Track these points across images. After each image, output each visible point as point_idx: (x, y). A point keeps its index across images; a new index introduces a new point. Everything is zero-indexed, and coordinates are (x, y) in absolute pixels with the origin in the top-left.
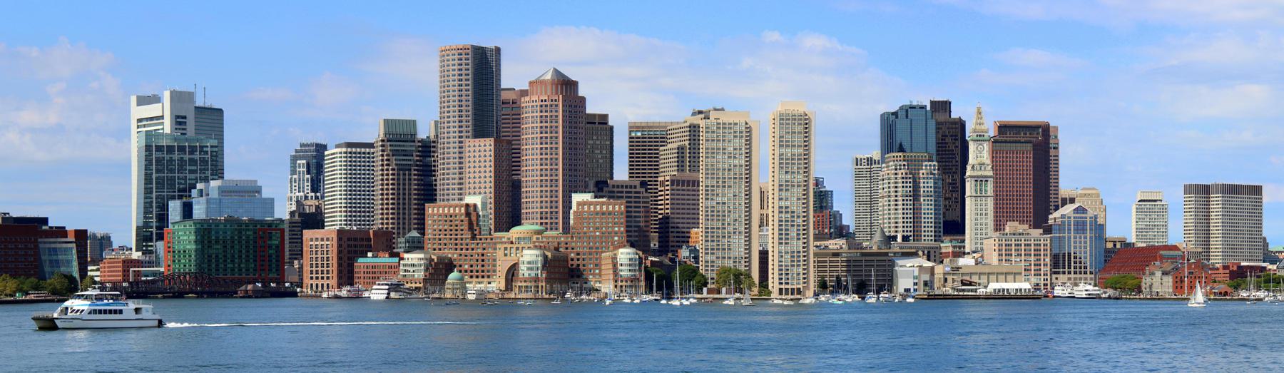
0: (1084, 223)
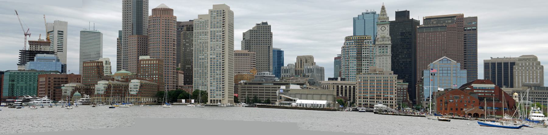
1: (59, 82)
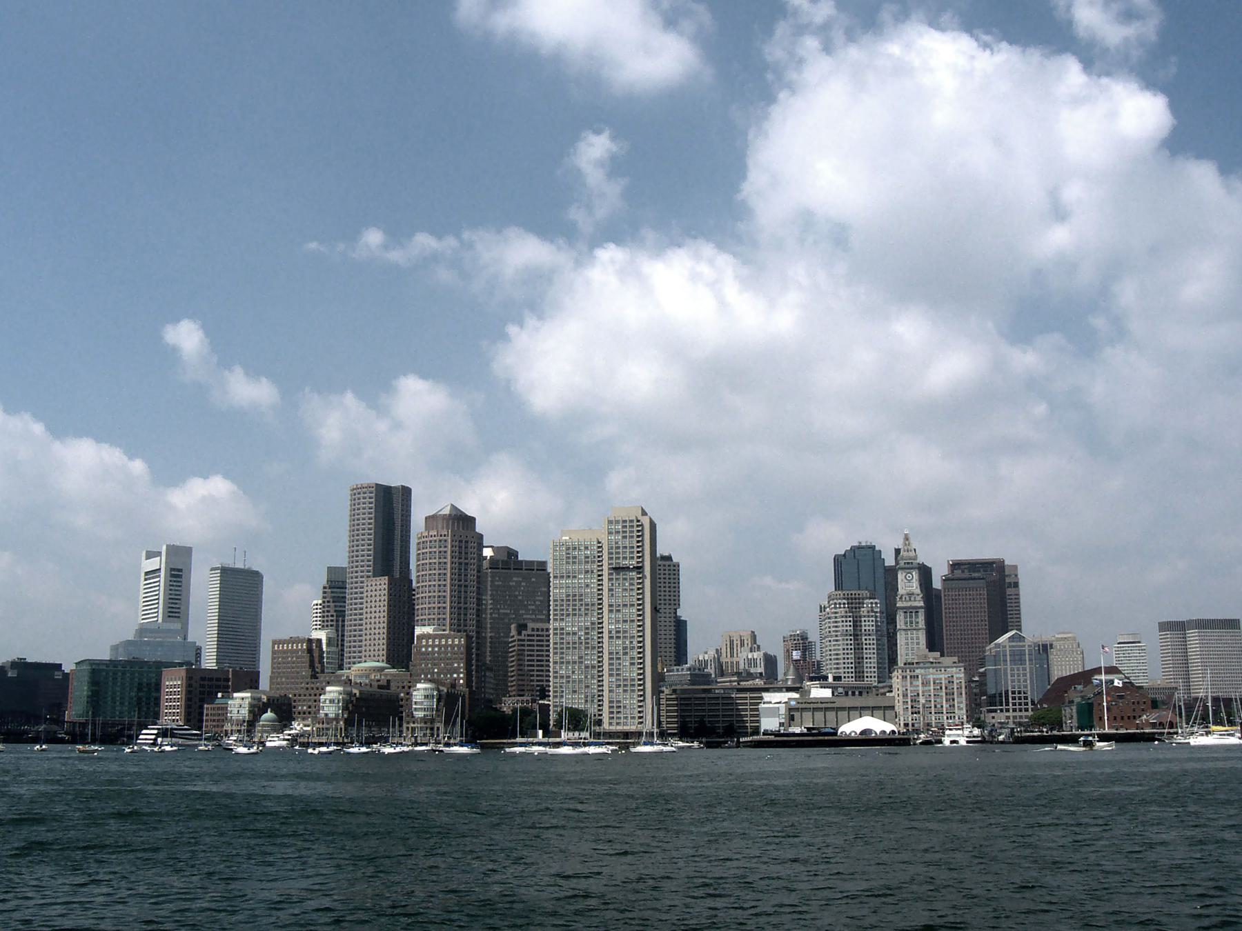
0: (1022, 653)
1: (210, 687)
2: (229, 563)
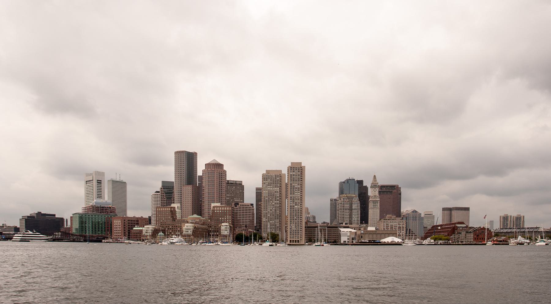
2: (114, 179)
